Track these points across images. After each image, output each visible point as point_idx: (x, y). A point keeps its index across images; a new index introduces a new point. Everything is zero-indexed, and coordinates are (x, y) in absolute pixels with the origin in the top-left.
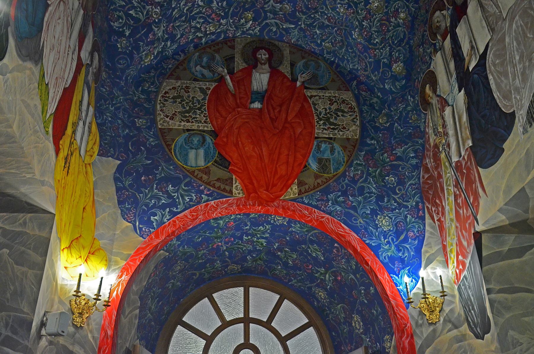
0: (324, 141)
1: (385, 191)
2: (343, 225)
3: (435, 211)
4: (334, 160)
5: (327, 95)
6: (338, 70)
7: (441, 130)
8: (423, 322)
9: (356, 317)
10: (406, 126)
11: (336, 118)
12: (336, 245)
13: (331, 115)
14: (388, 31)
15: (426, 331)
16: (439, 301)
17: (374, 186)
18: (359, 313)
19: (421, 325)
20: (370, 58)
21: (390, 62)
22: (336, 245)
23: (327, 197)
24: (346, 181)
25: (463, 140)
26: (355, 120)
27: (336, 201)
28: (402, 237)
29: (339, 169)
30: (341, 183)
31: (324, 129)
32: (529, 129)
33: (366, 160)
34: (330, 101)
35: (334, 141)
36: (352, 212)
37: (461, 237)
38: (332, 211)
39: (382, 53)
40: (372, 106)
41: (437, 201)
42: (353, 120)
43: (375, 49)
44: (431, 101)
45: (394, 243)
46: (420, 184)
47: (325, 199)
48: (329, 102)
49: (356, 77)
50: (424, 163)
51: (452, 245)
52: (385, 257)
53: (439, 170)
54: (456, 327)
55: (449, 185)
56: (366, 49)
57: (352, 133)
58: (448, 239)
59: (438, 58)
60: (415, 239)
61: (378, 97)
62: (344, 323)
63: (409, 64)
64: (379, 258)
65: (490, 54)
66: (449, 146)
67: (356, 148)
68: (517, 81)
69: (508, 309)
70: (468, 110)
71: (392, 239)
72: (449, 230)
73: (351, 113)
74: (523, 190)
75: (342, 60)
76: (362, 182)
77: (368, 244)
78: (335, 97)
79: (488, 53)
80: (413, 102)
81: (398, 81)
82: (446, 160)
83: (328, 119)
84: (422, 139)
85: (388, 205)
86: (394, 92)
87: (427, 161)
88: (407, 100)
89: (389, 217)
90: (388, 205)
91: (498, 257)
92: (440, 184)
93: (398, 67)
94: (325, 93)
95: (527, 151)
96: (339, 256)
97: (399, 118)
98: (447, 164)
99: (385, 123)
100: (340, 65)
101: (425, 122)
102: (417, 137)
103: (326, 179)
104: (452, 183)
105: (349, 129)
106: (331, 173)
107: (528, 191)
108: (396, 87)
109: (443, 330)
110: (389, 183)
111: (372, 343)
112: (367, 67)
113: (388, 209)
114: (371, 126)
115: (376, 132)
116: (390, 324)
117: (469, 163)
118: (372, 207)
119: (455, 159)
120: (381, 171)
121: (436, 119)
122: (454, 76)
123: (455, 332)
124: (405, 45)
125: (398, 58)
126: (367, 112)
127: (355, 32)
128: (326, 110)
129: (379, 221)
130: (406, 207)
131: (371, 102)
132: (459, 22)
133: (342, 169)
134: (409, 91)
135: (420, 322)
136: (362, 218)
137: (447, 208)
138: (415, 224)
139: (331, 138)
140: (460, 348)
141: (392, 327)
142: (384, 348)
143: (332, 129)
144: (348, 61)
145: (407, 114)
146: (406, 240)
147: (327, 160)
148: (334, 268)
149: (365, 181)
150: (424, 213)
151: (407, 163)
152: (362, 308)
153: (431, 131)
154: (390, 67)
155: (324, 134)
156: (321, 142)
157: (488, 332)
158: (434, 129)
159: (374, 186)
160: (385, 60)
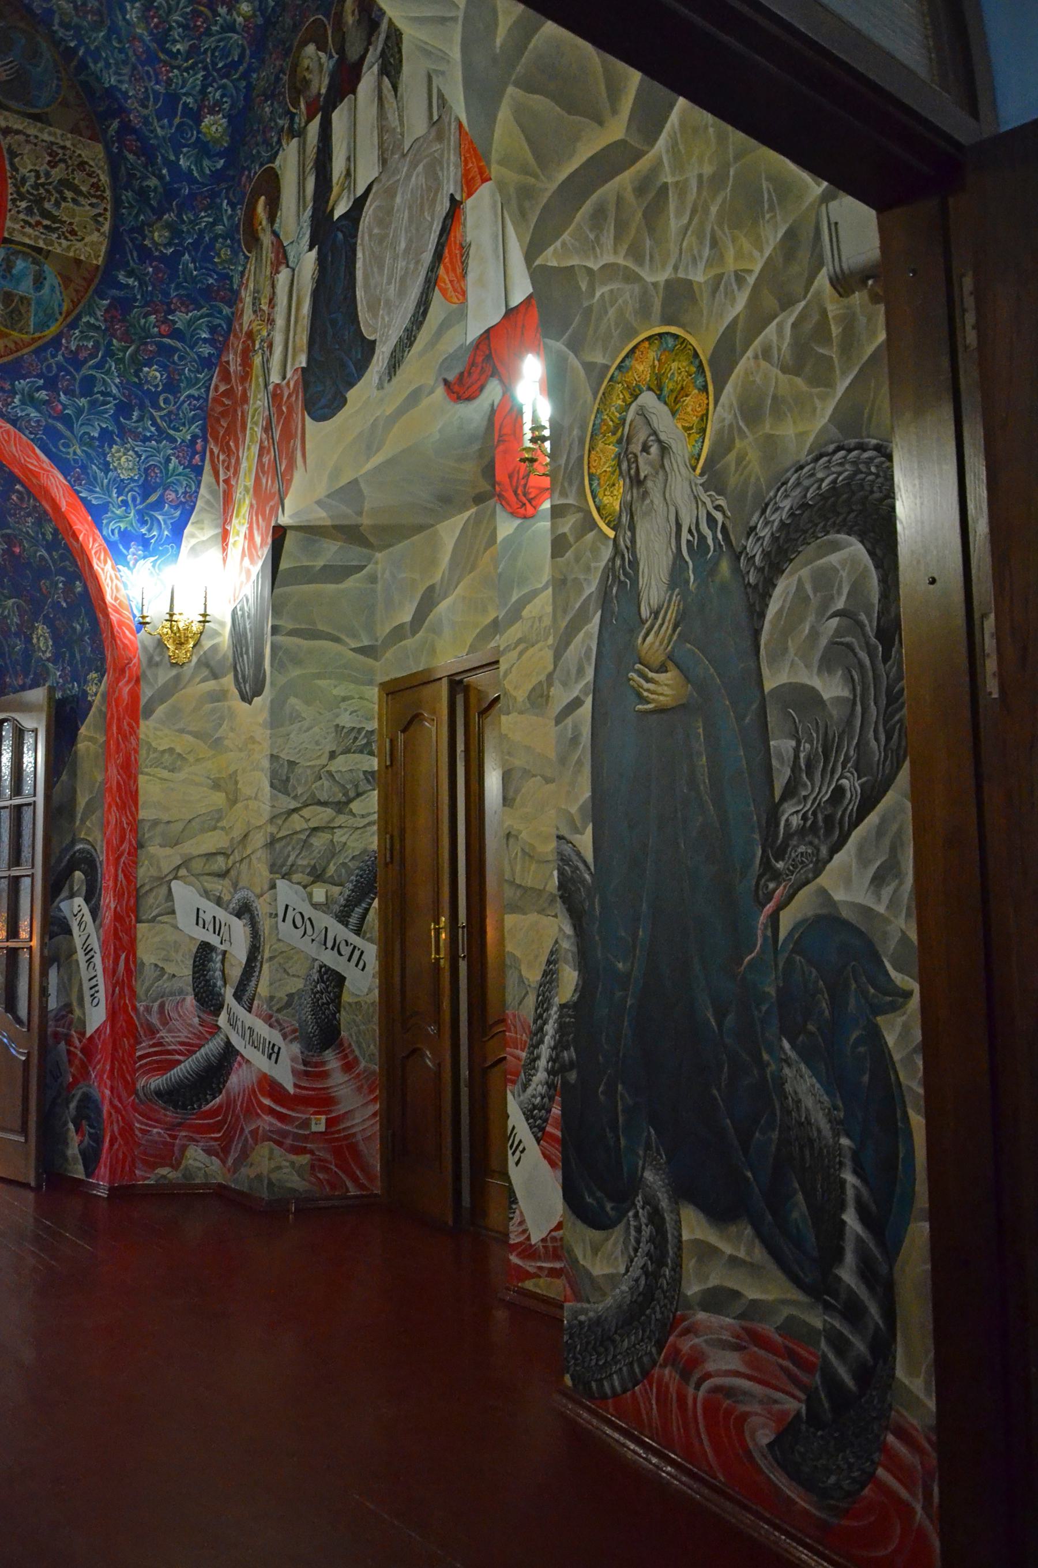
0: (24, 253)
1: (137, 396)
2: (38, 451)
3: (224, 461)
4: (39, 303)
5: (46, 137)
6: (82, 77)
7: (265, 307)
8: (161, 660)
9: (41, 628)
10: (206, 268)
11: (57, 204)
12: (18, 487)
13: (48, 191)
14: (208, 33)
15: (164, 676)
16: (194, 629)
17: (117, 380)
18: (50, 623)
19: (157, 665)
20: (157, 83)
21: (200, 108)
22: (18, 487)
23: (13, 385)
24: (60, 358)
25: (294, 349)
26: (100, 219)
27: (32, 399)
28: (153, 498)
29: (49, 327)
30: (46, 359)
31: (26, 222)
32: (386, 385)
33: (110, 320)
34: (50, 155)
35: (46, 258)
36: (60, 426)
37: (255, 526)
38: (18, 418)
39: (185, 82)
40: (143, 194)
41: (231, 444)
42: (95, 218)
43: (173, 67)
44: (261, 235)
45: (135, 506)
46: (206, 400)
47: (7, 387)
48: (48, 158)
49: (121, 111)
50: (224, 359)
51: (238, 534)
52: (113, 531)
53: (247, 385)
54: (215, 676)
55: (256, 424)
56: (151, 59)
57: (88, 249)
58: (235, 521)
59: (291, 149)
60: (176, 508)
61: (161, 177)
62: (17, 634)
63: (240, 123)
64: (101, 531)
65: (370, 206)
66: (271, 346)
67: (93, 287)
68: (393, 286)
69: (297, 661)
70: (316, 294)
71: (134, 499)
72: (239, 507)
73: (94, 201)
74: (355, 482)
75: (96, 56)
76: (90, 368)
77: (83, 500)
78: (64, 148)
79: (368, 204)
80: (231, 217)
81: (209, 157)
82: (260, 373)
83: (39, 201)
84: (231, 307)
85: (137, 428)
86: (194, 181)
87: (231, 356)
88: (219, 207)
89: (136, 453)
90: (137, 428)
91: (304, 575)
92: (242, 413)
93: (214, 126)
94: (41, 130)
95: (375, 420)
96: (22, 509)
97: (196, 245)
98: (261, 380)
99: (165, 246)
100: (87, 67)
101: (242, 273)
102: (223, 300)
103: (16, 343)
104: (262, 423)
105: (83, 239)
106: (27, 333)
107: (363, 485)
108: (201, 171)
109: (192, 677)
110: (147, 382)
111: (66, 682)
112: (147, 98)
113: (136, 436)
114: (134, 243)
115: (142, 261)
116: (102, 653)
117: (294, 398)
118: (104, 426)
119: (275, 378)
120: (137, 351)
121: (262, 280)
122: (308, 212)
123: (211, 685)
124: (238, 79)
125: (218, 103)
126: (132, 206)
127: (133, 8)
128: (38, 177)
129: (113, 455)
130: (173, 440)
131: (145, 184)
132: (341, 101)
133: (53, 330)
134: (228, 189)
135: (157, 659)
136: (80, 446)
137: (244, 465)
138: (181, 478)
139: (39, 250)
140: (213, 711)
141: (103, 659)
142: (85, 694)
143: (46, 227)
144: (108, 65)
145: (214, 239)
146: (158, 505)
147: (22, 299)
148: (9, 528)
149: (99, 366)
150: (203, 460)
151: (192, 348)
152: (55, 616)
153: (248, 300)
154: (197, 118)
155: (24, 234)
156: (17, 253)
157: (259, 695)
158: (255, 298)
159: (117, 380)
160: (190, 100)
